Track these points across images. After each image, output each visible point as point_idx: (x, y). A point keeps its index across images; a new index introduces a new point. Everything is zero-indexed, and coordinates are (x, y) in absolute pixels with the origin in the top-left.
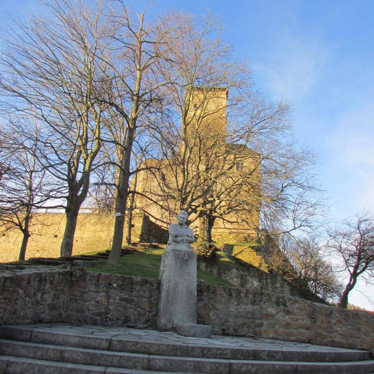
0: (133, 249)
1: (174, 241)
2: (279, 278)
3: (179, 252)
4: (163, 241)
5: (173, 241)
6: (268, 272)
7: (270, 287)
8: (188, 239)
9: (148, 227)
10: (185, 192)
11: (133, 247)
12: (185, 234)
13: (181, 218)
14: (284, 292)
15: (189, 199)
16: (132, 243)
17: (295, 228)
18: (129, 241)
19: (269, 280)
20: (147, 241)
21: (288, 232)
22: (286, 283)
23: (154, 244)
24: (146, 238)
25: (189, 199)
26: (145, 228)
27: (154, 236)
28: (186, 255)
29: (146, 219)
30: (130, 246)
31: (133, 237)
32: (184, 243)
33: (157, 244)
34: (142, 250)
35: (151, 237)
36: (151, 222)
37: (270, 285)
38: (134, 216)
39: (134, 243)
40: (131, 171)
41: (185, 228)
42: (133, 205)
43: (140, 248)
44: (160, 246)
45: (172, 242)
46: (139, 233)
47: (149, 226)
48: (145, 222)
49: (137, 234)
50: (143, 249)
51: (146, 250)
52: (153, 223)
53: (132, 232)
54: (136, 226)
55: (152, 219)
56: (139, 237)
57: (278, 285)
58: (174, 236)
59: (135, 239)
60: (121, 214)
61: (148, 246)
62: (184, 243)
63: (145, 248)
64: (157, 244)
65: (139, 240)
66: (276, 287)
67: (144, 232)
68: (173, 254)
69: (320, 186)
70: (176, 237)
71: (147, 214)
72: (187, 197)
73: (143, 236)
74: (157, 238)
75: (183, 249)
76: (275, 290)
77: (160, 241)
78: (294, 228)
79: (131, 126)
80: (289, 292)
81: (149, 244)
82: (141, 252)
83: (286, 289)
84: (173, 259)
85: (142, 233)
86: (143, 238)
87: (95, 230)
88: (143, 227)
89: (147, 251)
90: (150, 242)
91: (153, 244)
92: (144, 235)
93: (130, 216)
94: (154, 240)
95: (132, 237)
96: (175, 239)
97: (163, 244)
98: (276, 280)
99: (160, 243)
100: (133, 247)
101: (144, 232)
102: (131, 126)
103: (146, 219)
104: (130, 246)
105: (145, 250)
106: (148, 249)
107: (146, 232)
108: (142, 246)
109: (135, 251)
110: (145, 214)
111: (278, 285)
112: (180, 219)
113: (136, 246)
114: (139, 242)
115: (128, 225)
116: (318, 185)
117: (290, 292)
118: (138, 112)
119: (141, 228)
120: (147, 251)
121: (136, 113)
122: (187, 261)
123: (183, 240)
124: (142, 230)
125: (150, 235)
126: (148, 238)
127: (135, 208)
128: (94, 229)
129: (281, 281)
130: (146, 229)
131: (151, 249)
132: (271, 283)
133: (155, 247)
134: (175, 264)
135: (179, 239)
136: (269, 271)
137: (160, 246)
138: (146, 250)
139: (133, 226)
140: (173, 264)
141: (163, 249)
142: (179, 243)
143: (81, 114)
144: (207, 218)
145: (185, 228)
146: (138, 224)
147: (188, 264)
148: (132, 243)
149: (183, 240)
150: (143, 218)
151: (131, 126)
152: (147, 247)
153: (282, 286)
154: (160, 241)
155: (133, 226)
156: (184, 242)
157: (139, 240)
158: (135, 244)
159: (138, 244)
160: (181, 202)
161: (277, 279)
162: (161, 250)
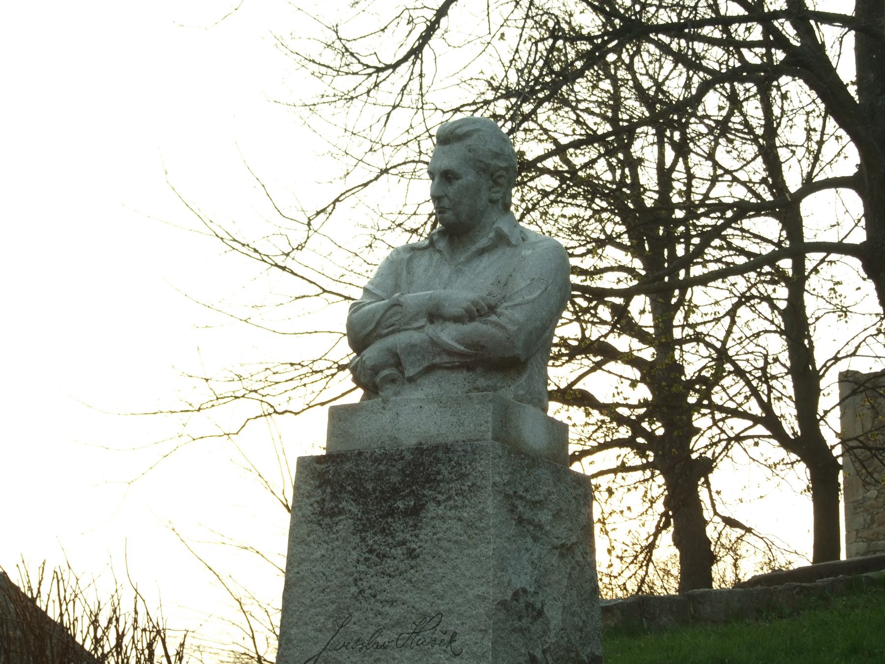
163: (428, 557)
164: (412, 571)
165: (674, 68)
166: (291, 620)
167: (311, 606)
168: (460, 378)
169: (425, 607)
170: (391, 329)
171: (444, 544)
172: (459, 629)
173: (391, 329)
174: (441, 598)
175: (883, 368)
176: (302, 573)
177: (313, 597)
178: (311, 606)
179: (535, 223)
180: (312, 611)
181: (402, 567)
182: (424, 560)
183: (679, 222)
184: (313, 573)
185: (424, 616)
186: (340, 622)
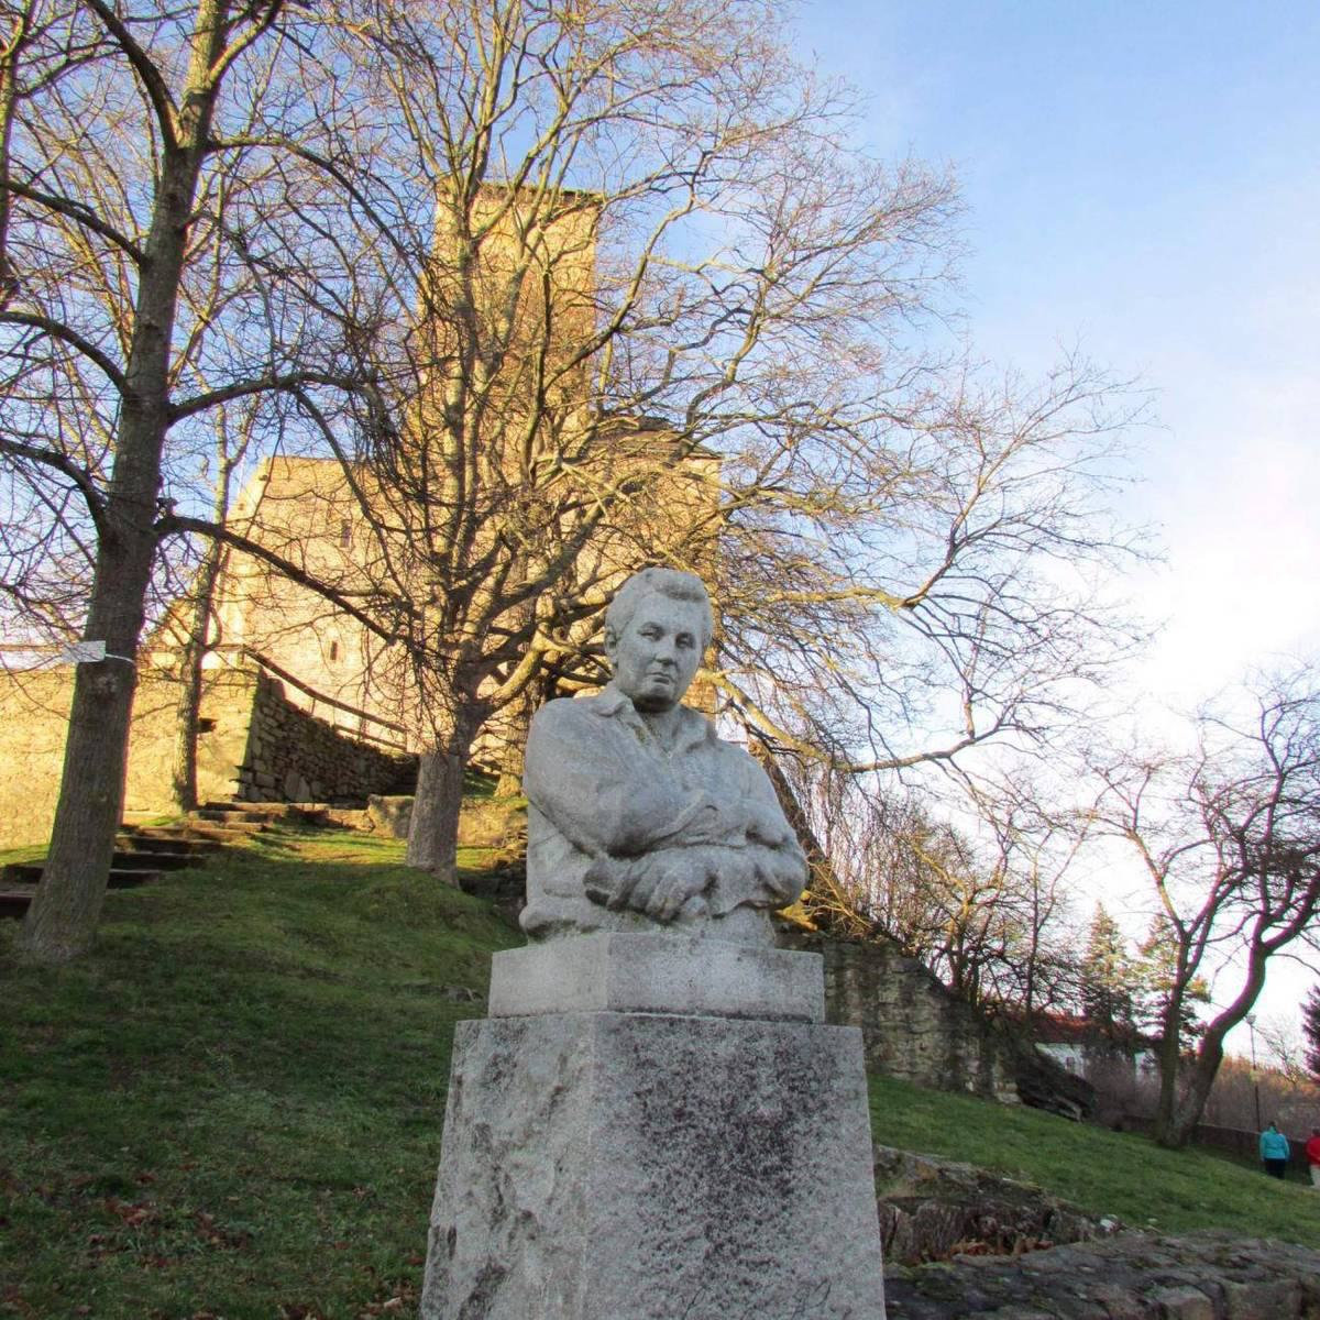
0: (203, 835)
1: (613, 895)
2: (893, 963)
3: (681, 1040)
4: (345, 790)
5: (596, 899)
6: (809, 925)
7: (856, 1007)
8: (759, 874)
9: (279, 733)
10: (461, 566)
11: (209, 826)
12: (727, 815)
13: (656, 633)
14: (916, 1028)
15: (481, 598)
16: (201, 802)
17: (973, 739)
18: (186, 791)
19: (849, 974)
20: (272, 793)
21: (947, 755)
22: (926, 986)
23: (308, 807)
24: (269, 779)
25: (481, 598)
26: (264, 735)
27: (303, 769)
28: (764, 1073)
29: (269, 694)
30: (195, 820)
31: (211, 775)
32: (718, 917)
33: (319, 807)
34: (248, 843)
35: (292, 775)
36: (292, 710)
37: (854, 997)
38: (215, 683)
39: (210, 806)
40: (177, 397)
41: (693, 747)
42: (205, 629)
43: (238, 834)
44: (335, 815)
45: (581, 908)
46: (238, 755)
47: (280, 726)
48: (266, 710)
49: (230, 763)
50: (253, 837)
51: (271, 836)
52: (302, 715)
53: (203, 754)
54: (220, 726)
55: (295, 696)
56: (237, 773)
57: (891, 995)
58: (608, 837)
59: (217, 784)
60: (108, 651)
61: (278, 819)
62: (718, 917)
63: (264, 830)
64: (319, 807)
65: (234, 787)
66: (884, 1004)
67: (258, 751)
68: (615, 1069)
69: (1143, 536)
70: (631, 847)
71: (270, 673)
72: (474, 587)
73: (255, 772)
74: (321, 779)
75: (716, 997)
76: (876, 1017)
77: (330, 792)
78: (967, 737)
79: (184, 139)
80: (936, 1022)
81: (279, 808)
82: (243, 855)
83: (925, 1013)
84: (619, 1141)
85: (251, 756)
86: (251, 779)
87: (29, 745)
88: (254, 730)
89: (272, 844)
90: (285, 799)
91: (299, 805)
92: (258, 765)
93: (190, 679)
94: (304, 787)
95: (201, 774)
96: (619, 871)
97: (350, 808)
98: (880, 970)
99: (331, 801)
100: (209, 826)
101: (258, 751)
102: (184, 139)
103: (269, 694)
104: (195, 820)
105: (264, 841)
106: (277, 832)
107: (267, 754)
108: (251, 818)
109: (213, 845)
110: (262, 672)
111: (891, 995)
112: (646, 646)
113: (222, 819)
114: (237, 797)
115: (181, 720)
116: (1132, 534)
117: (942, 1021)
118: (227, 54)
119: (246, 734)
120: (272, 844)
121: (211, 66)
122: (777, 1137)
123: (710, 887)
124: (249, 746)
125: (288, 766)
126: (277, 780)
127: (215, 646)
128: (23, 739)
129: (903, 977)
130: (272, 739)
131: (289, 830)
132: (860, 986)
133: (313, 823)
134: (652, 1207)
135: (672, 870)
136: (814, 920)
137: (335, 815)
138: (271, 836)
139: (207, 725)
140: (627, 1204)
141: (350, 828)
142: (672, 918)
143: (210, 641)
144: (540, 694)
145: (693, 747)
146: (232, 714)
147: (798, 1176)
148: (201, 802)
149: (710, 887)
150: (253, 690)
151: (179, 135)
152: (270, 825)
153: (907, 1000)
154: (330, 792)
155: (207, 725)
156: (726, 906)
157: (234, 787)
158: (215, 811)
159: (232, 808)
160: (444, 610)
161: (886, 965)
162: (340, 836)
163: (804, 1193)
164: (786, 1214)
165: (569, 442)
166: (608, 1299)
167: (642, 1274)
168: (660, 832)
169: (805, 1271)
170: (701, 838)
171: (821, 1173)
172: (855, 1305)
173: (701, 838)
174: (825, 1256)
175: (1314, 981)
176: (622, 1215)
177: (645, 1257)
178: (642, 1274)
179: (20, 350)
180: (645, 1282)
181: (773, 1209)
182: (799, 1197)
183: (1270, 850)
184: (641, 1216)
185: (808, 1284)
186: (689, 1299)
